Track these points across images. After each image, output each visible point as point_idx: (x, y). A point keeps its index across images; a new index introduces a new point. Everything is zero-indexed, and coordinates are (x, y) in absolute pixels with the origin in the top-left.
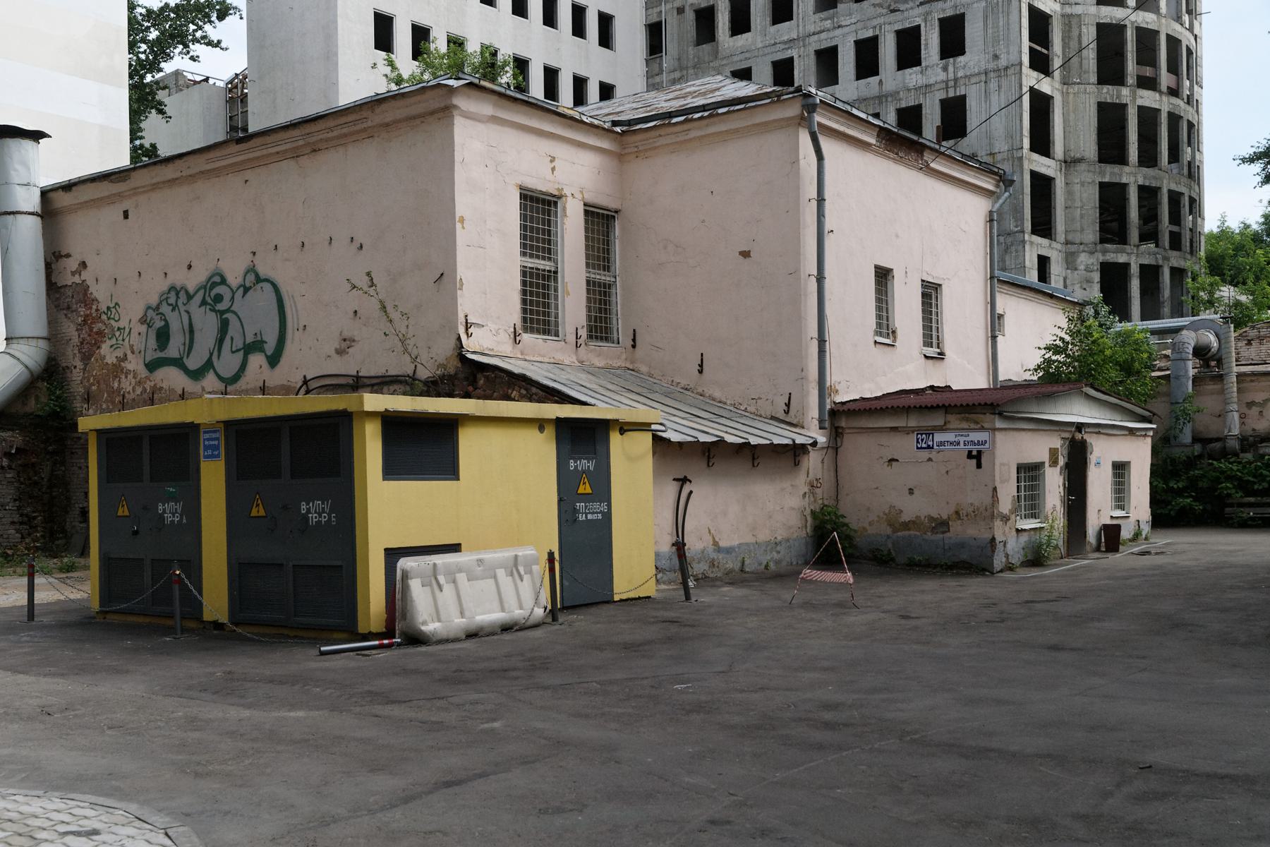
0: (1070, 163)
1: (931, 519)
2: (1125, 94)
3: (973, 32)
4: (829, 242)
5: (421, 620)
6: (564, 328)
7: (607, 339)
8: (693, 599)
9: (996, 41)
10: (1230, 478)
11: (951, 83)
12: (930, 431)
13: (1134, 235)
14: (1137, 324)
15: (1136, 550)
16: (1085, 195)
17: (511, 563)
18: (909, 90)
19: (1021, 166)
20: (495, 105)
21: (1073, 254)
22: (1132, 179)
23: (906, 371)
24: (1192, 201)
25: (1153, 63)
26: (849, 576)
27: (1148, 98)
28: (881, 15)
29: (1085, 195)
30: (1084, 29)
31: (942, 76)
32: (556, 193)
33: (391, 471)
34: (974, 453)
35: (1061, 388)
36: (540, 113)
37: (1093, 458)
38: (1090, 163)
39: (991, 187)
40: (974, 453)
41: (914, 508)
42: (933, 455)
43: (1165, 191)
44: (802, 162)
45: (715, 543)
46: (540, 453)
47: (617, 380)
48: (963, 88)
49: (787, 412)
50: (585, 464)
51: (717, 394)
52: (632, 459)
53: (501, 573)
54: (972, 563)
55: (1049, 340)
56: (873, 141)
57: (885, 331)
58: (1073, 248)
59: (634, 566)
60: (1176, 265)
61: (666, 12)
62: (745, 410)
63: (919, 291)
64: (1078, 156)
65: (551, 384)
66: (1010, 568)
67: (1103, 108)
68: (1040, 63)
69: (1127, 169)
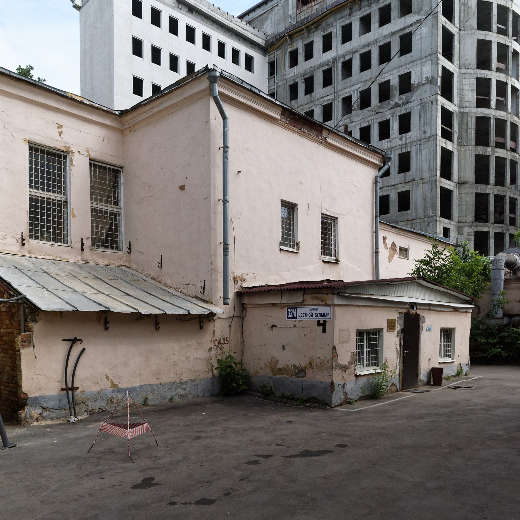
0: (461, 184)
1: (295, 366)
2: (489, 150)
3: (414, 121)
6: (71, 238)
9: (425, 124)
11: (404, 146)
12: (295, 306)
13: (492, 218)
19: (436, 184)
21: (461, 227)
25: (504, 136)
27: (500, 153)
29: (468, 199)
30: (470, 119)
31: (399, 143)
34: (322, 322)
36: (37, 90)
37: (425, 326)
38: (471, 184)
40: (322, 322)
41: (287, 359)
42: (297, 323)
43: (508, 197)
45: (114, 386)
48: (409, 148)
51: (168, 282)
55: (421, 258)
56: (278, 117)
58: (462, 224)
64: (465, 180)
66: (348, 402)
68: (447, 135)
69: (489, 186)
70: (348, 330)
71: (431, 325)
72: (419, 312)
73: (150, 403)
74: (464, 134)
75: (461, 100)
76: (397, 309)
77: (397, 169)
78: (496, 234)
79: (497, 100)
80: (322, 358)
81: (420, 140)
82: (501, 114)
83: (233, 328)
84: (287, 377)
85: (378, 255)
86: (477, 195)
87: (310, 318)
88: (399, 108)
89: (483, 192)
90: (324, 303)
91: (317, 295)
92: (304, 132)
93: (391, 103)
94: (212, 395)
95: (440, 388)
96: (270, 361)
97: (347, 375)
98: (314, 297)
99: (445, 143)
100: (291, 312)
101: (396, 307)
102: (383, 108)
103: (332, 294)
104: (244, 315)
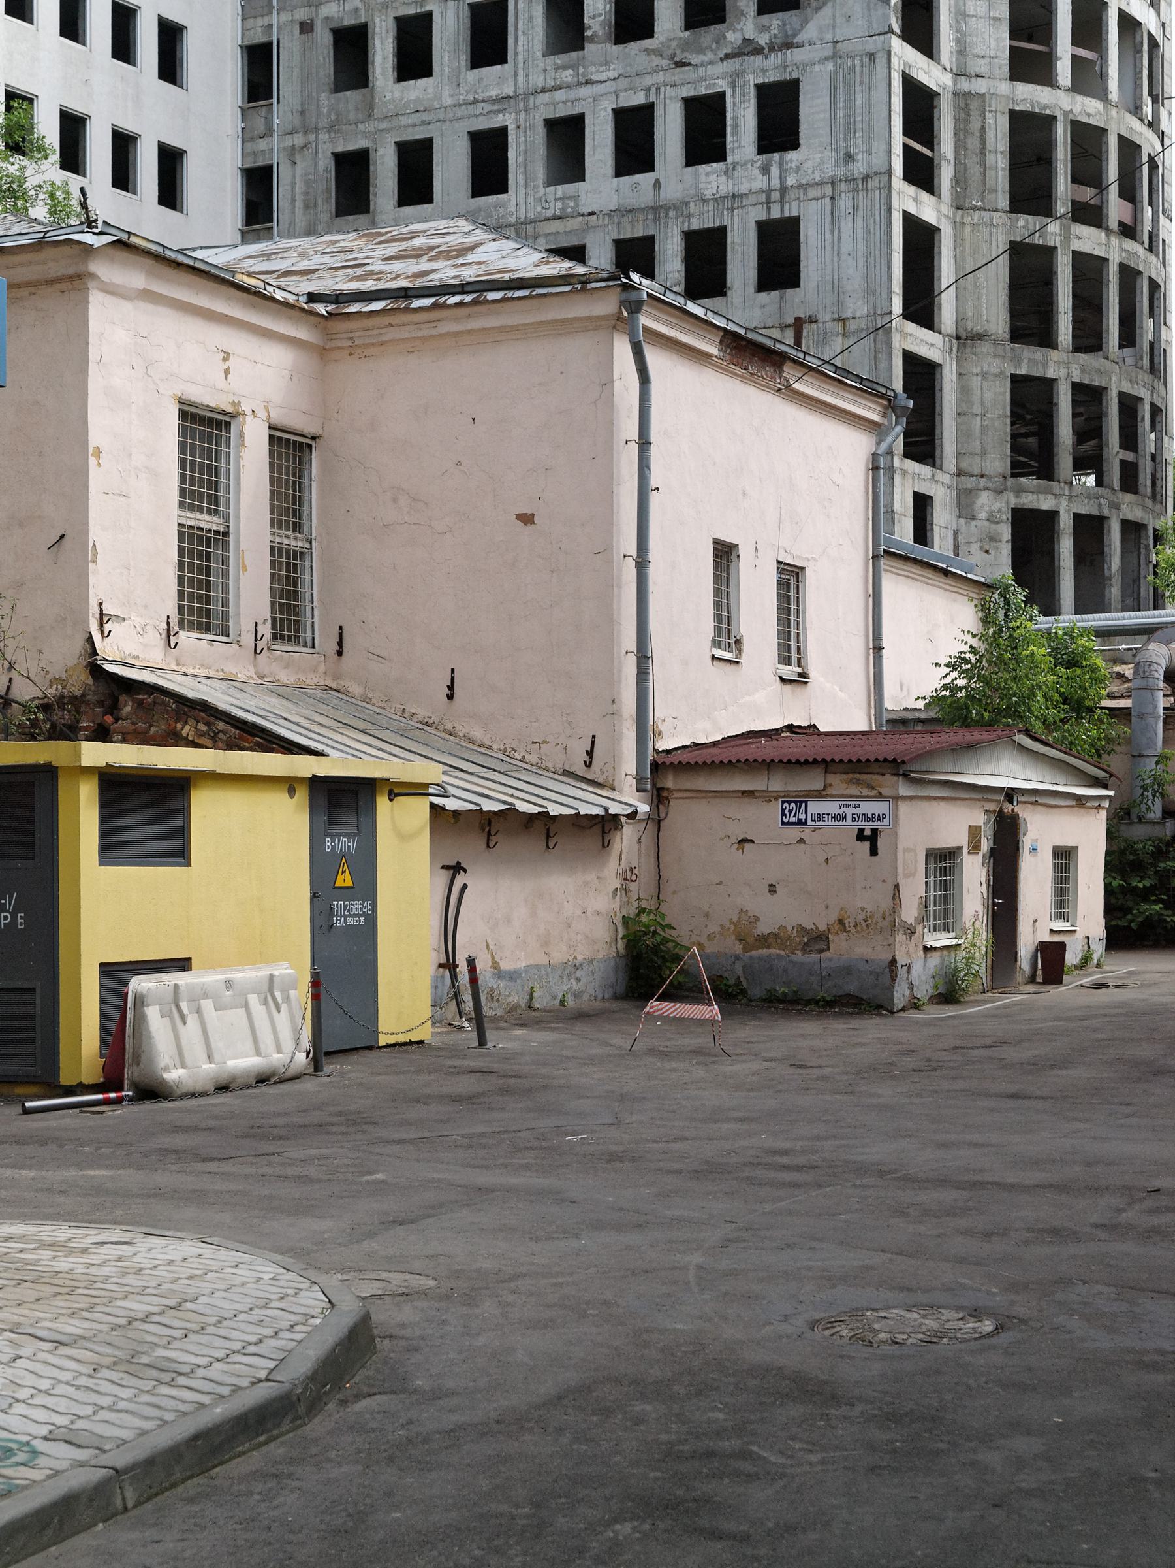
0: (966, 339)
1: (802, 930)
2: (1053, 232)
3: (812, 111)
4: (655, 501)
5: (162, 1065)
6: (238, 623)
7: (296, 640)
8: (490, 1045)
9: (850, 131)
11: (776, 196)
12: (802, 799)
14: (1067, 619)
15: (1086, 981)
16: (988, 395)
17: (265, 987)
18: (705, 201)
19: (889, 343)
20: (150, 274)
22: (1063, 373)
24: (1156, 411)
25: (1099, 184)
26: (713, 1011)
27: (1088, 239)
28: (658, 70)
29: (988, 395)
30: (990, 120)
31: (760, 182)
32: (229, 409)
33: (110, 853)
34: (867, 833)
35: (985, 736)
36: (212, 285)
37: (1026, 842)
38: (997, 343)
39: (875, 417)
40: (867, 833)
41: (778, 914)
42: (806, 833)
46: (287, 823)
47: (323, 708)
48: (795, 204)
49: (588, 765)
50: (344, 844)
51: (477, 733)
52: (403, 837)
53: (253, 1000)
54: (861, 997)
56: (714, 350)
57: (724, 640)
58: (969, 483)
59: (405, 1000)
60: (1129, 517)
61: (280, 27)
62: (523, 760)
63: (773, 577)
64: (978, 329)
65: (250, 718)
66: (915, 1005)
67: (1017, 250)
68: (920, 172)
69: (1054, 355)
70: (914, 851)
71: (1036, 840)
73: (536, 1006)
74: (974, 170)
75: (961, 51)
77: (752, 274)
79: (1075, 58)
80: (869, 908)
81: (833, 184)
82: (1088, 108)
84: (782, 953)
85: (881, 657)
86: (1018, 382)
88: (758, 60)
91: (857, 776)
93: (730, 36)
94: (616, 997)
96: (735, 919)
99: (916, 200)
100: (790, 811)
101: (984, 799)
102: (701, 51)
104: (662, 816)
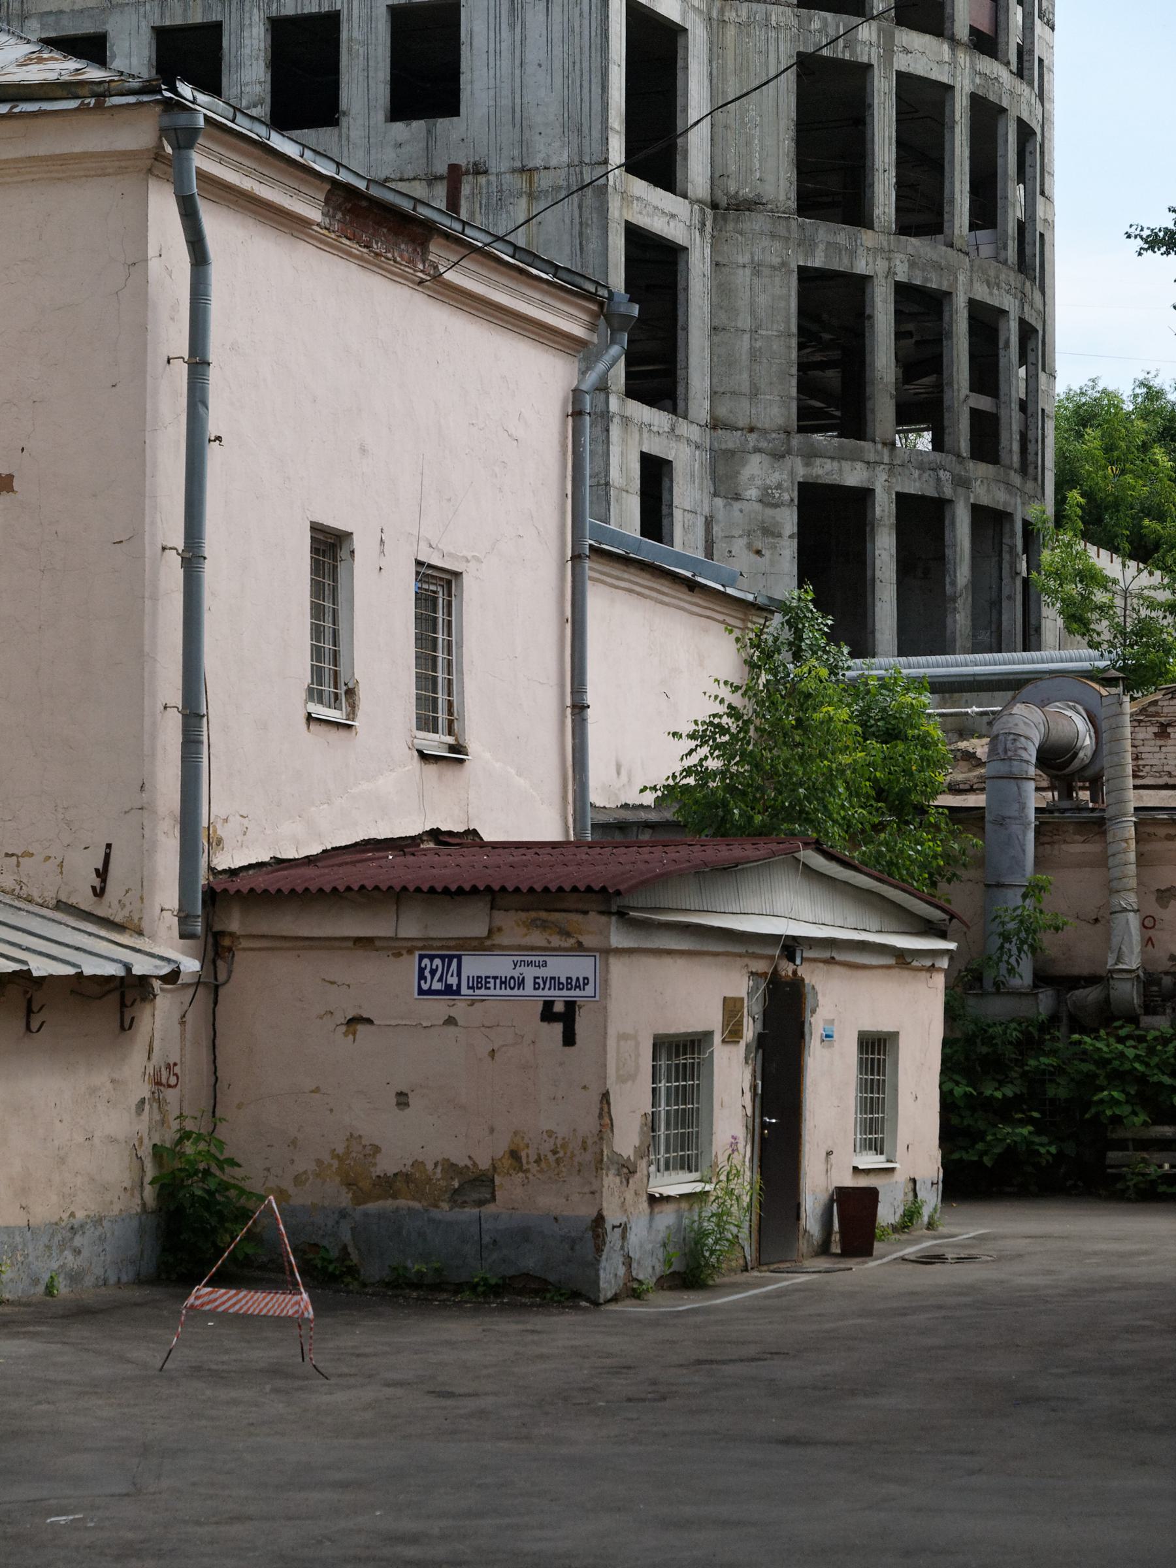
0: (726, 209)
1: (450, 1168)
4: (214, 456)
10: (1119, 1077)
12: (452, 952)
14: (886, 663)
15: (910, 1251)
16: (763, 300)
22: (881, 266)
23: (369, 792)
26: (300, 1303)
27: (922, 55)
29: (763, 300)
34: (559, 1008)
35: (750, 852)
37: (816, 1023)
39: (578, 331)
40: (559, 1008)
41: (412, 1141)
42: (459, 1008)
44: (154, 265)
49: (99, 893)
54: (546, 1277)
56: (314, 214)
57: (328, 689)
58: (731, 440)
60: (985, 501)
64: (746, 192)
66: (633, 1291)
69: (868, 238)
70: (635, 1037)
72: (804, 971)
76: (746, 960)
77: (381, 92)
78: (903, 500)
83: (188, 1027)
87: (515, 992)
89: (840, 264)
90: (571, 942)
91: (543, 915)
92: (377, 254)
94: (140, 1281)
95: (872, 1264)
96: (340, 1150)
97: (632, 1192)
98: (534, 920)
100: (433, 972)
103: (602, 913)
104: (222, 977)
